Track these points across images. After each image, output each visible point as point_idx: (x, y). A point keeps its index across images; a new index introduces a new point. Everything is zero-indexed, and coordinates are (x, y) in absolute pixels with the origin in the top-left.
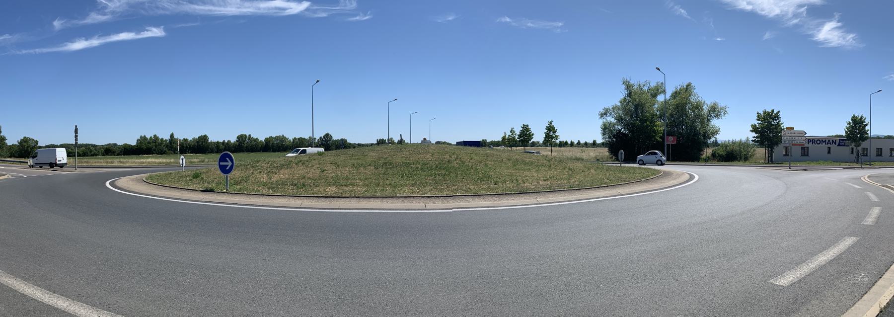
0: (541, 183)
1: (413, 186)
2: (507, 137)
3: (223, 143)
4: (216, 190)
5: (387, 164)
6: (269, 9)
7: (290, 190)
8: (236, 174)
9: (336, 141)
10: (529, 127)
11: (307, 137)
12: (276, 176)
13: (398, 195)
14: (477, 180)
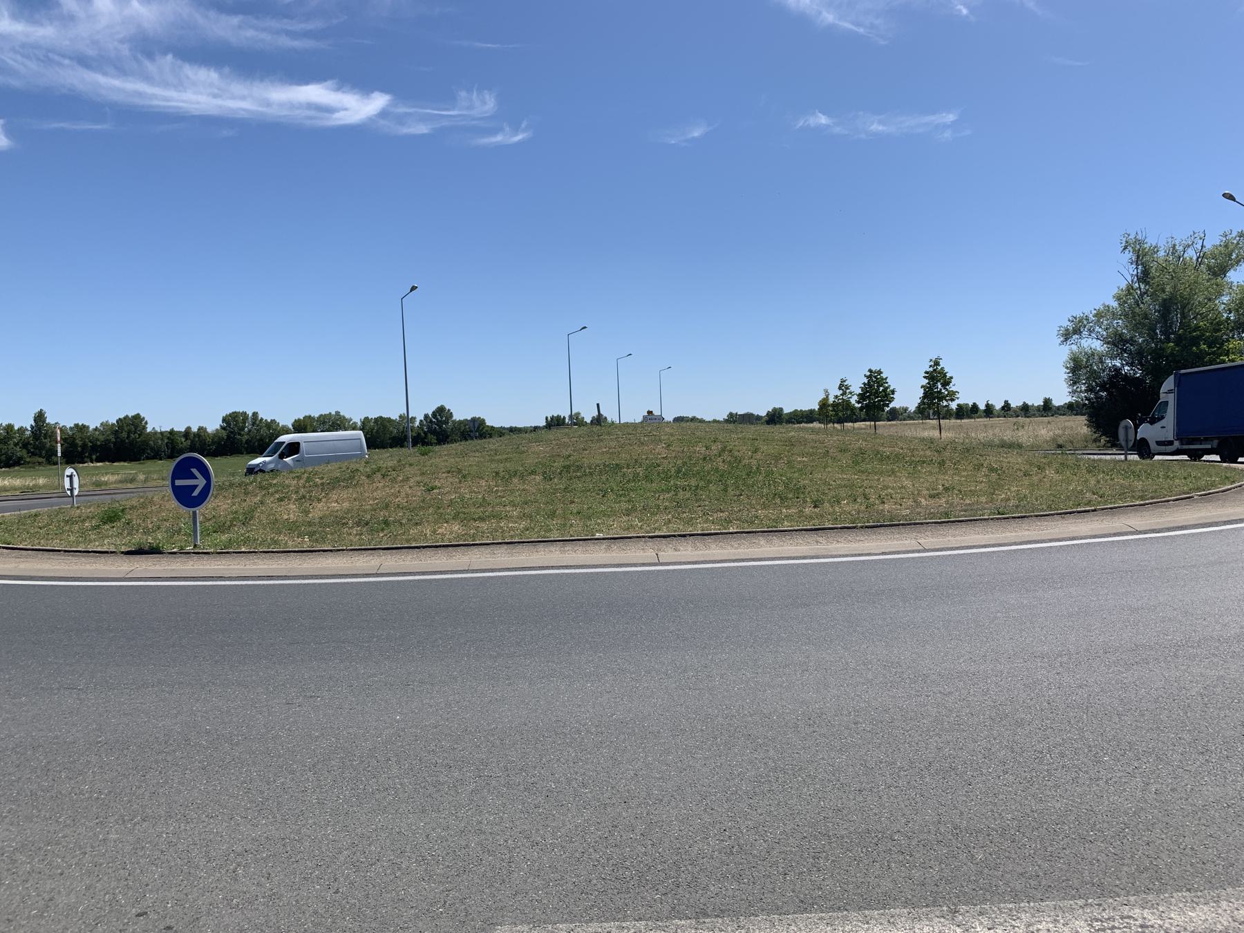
0: (924, 502)
1: (628, 515)
2: (831, 400)
3: (187, 433)
4: (167, 548)
5: (571, 469)
6: (292, 106)
7: (353, 535)
8: (217, 506)
9: (460, 422)
10: (884, 376)
11: (395, 416)
12: (320, 505)
13: (598, 535)
14: (774, 498)
